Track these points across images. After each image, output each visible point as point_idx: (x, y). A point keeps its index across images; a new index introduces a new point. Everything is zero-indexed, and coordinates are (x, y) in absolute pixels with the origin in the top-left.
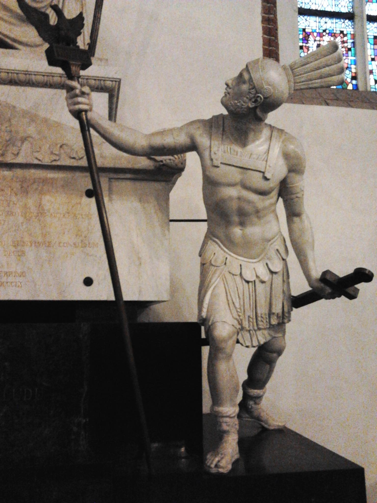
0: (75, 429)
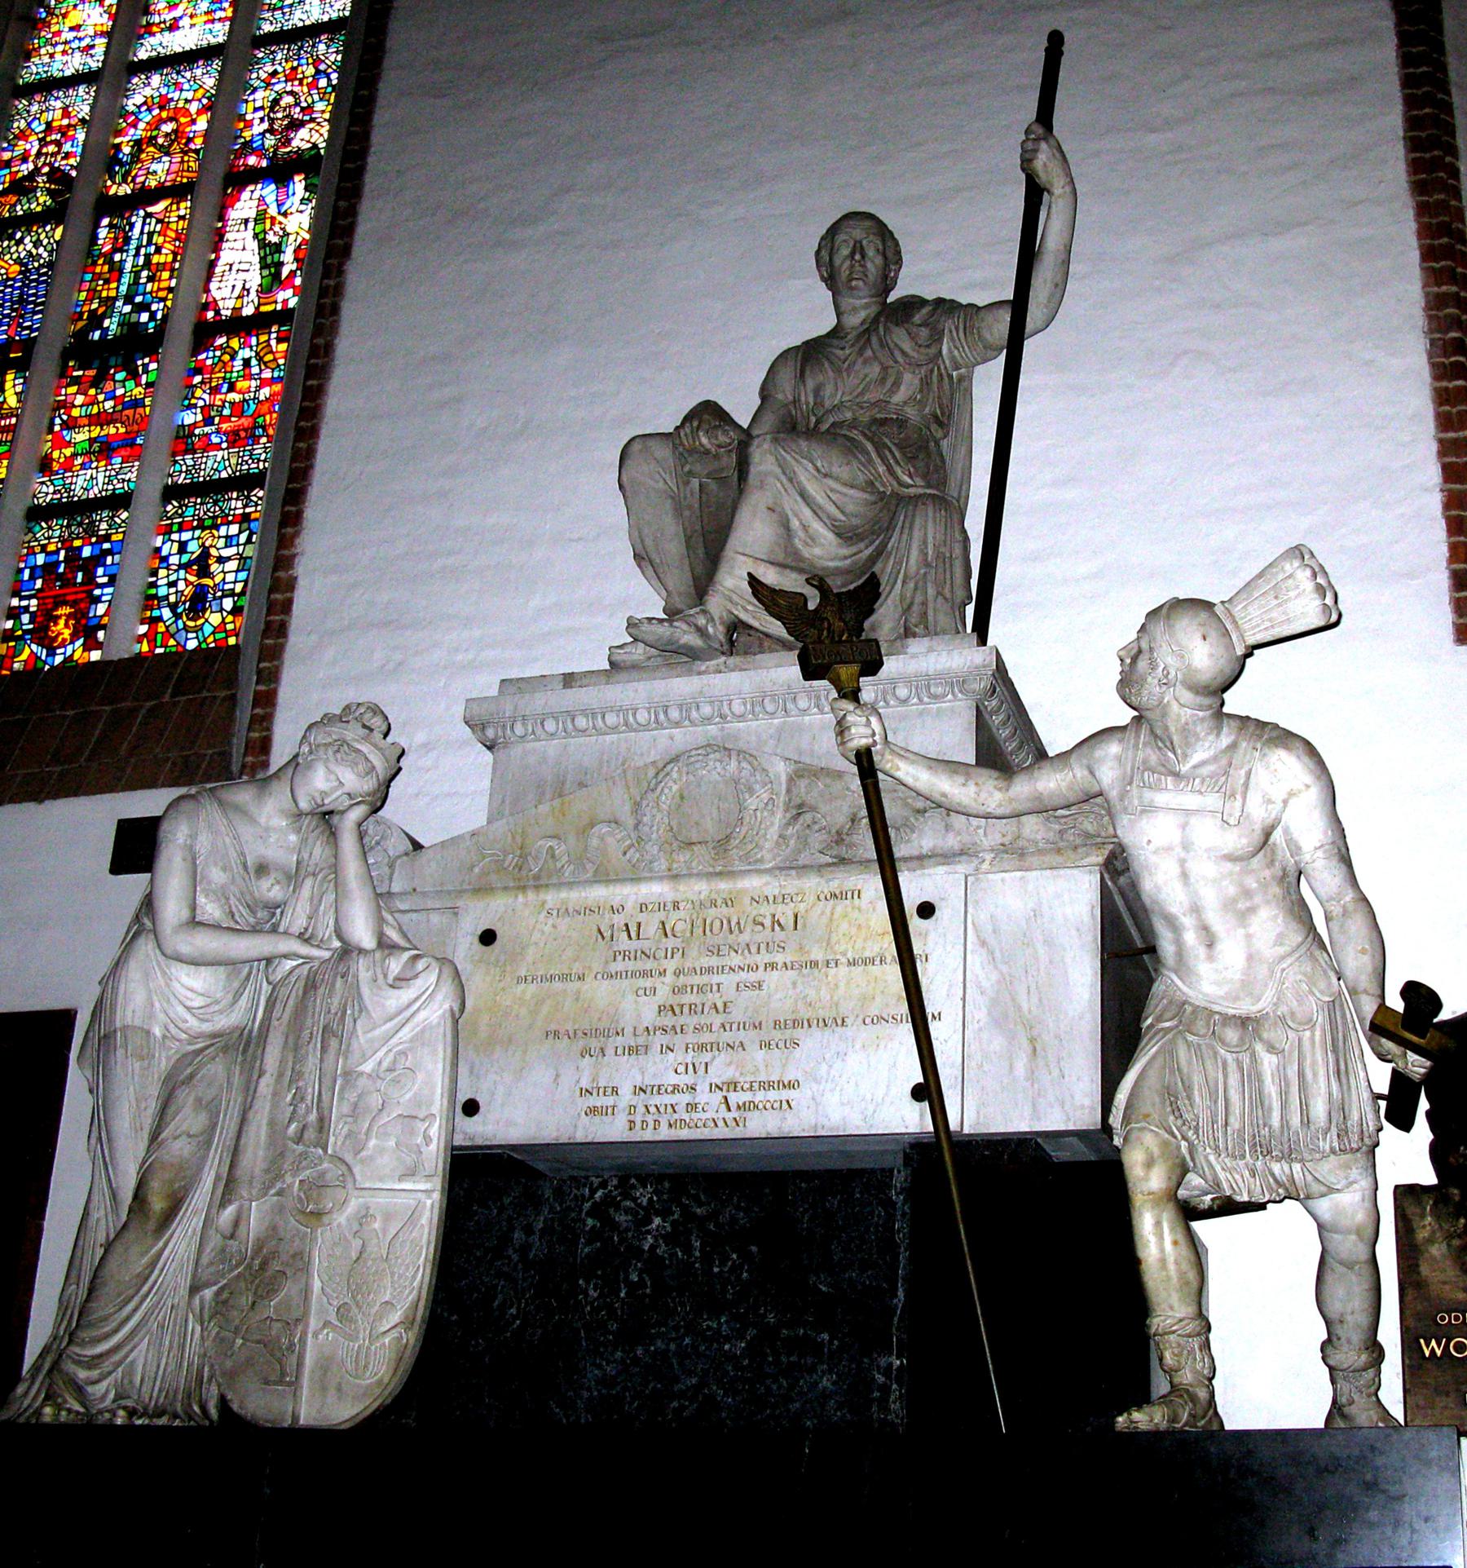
0: (880, 1378)
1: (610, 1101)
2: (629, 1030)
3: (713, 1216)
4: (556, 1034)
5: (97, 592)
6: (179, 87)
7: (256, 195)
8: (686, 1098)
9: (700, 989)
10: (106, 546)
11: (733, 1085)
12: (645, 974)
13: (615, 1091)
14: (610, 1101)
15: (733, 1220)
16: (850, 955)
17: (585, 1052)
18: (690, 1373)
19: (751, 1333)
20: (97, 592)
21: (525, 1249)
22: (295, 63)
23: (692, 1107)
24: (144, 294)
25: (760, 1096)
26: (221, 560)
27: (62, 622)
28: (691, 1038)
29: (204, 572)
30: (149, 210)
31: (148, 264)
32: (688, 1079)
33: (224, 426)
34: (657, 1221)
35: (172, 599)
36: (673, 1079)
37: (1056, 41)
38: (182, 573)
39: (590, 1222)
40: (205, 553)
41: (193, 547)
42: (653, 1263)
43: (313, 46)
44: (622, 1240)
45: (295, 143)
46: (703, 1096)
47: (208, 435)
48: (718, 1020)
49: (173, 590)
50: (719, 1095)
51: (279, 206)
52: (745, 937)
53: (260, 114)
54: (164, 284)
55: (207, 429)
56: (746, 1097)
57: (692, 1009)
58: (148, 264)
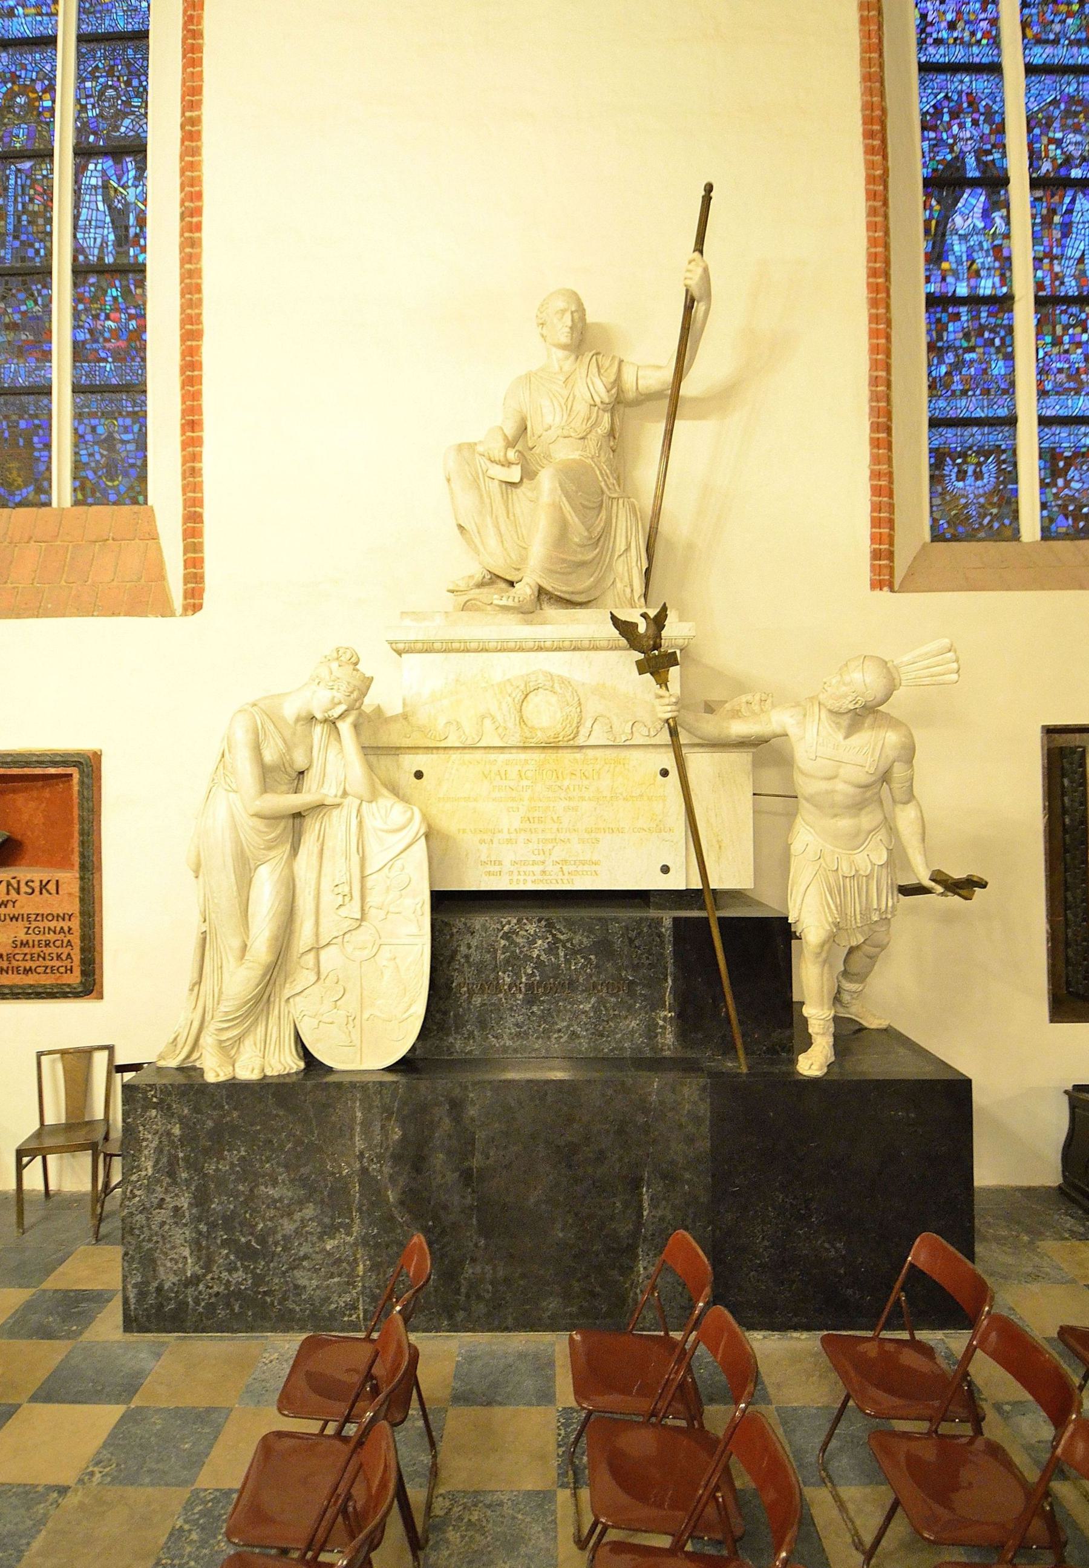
0: (661, 1023)
1: (497, 868)
2: (505, 830)
3: (570, 940)
5: (36, 454)
6: (24, 67)
7: (99, 167)
8: (541, 867)
10: (37, 422)
11: (565, 861)
12: (513, 799)
13: (500, 863)
14: (497, 868)
15: (581, 943)
16: (625, 795)
17: (482, 841)
18: (563, 1020)
19: (593, 1000)
20: (36, 454)
21: (467, 957)
22: (112, 63)
23: (544, 872)
24: (28, 234)
25: (580, 868)
26: (123, 442)
27: (15, 473)
28: (541, 836)
29: (111, 448)
30: (19, 166)
31: (25, 210)
32: (541, 858)
33: (107, 345)
34: (540, 942)
35: (93, 464)
36: (534, 858)
37: (709, 188)
38: (96, 448)
39: (503, 942)
40: (110, 437)
41: (100, 430)
42: (539, 964)
43: (124, 50)
44: (521, 952)
45: (123, 129)
46: (549, 868)
47: (97, 351)
49: (92, 459)
51: (119, 180)
52: (566, 783)
53: (92, 100)
54: (41, 229)
55: (95, 346)
56: (572, 868)
57: (540, 820)
58: (25, 210)
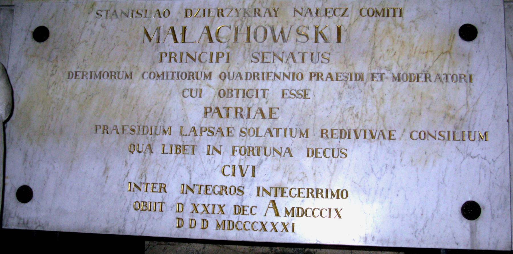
2: (175, 130)
4: (106, 129)
9: (246, 94)
46: (250, 199)
48: (264, 125)
50: (267, 200)
